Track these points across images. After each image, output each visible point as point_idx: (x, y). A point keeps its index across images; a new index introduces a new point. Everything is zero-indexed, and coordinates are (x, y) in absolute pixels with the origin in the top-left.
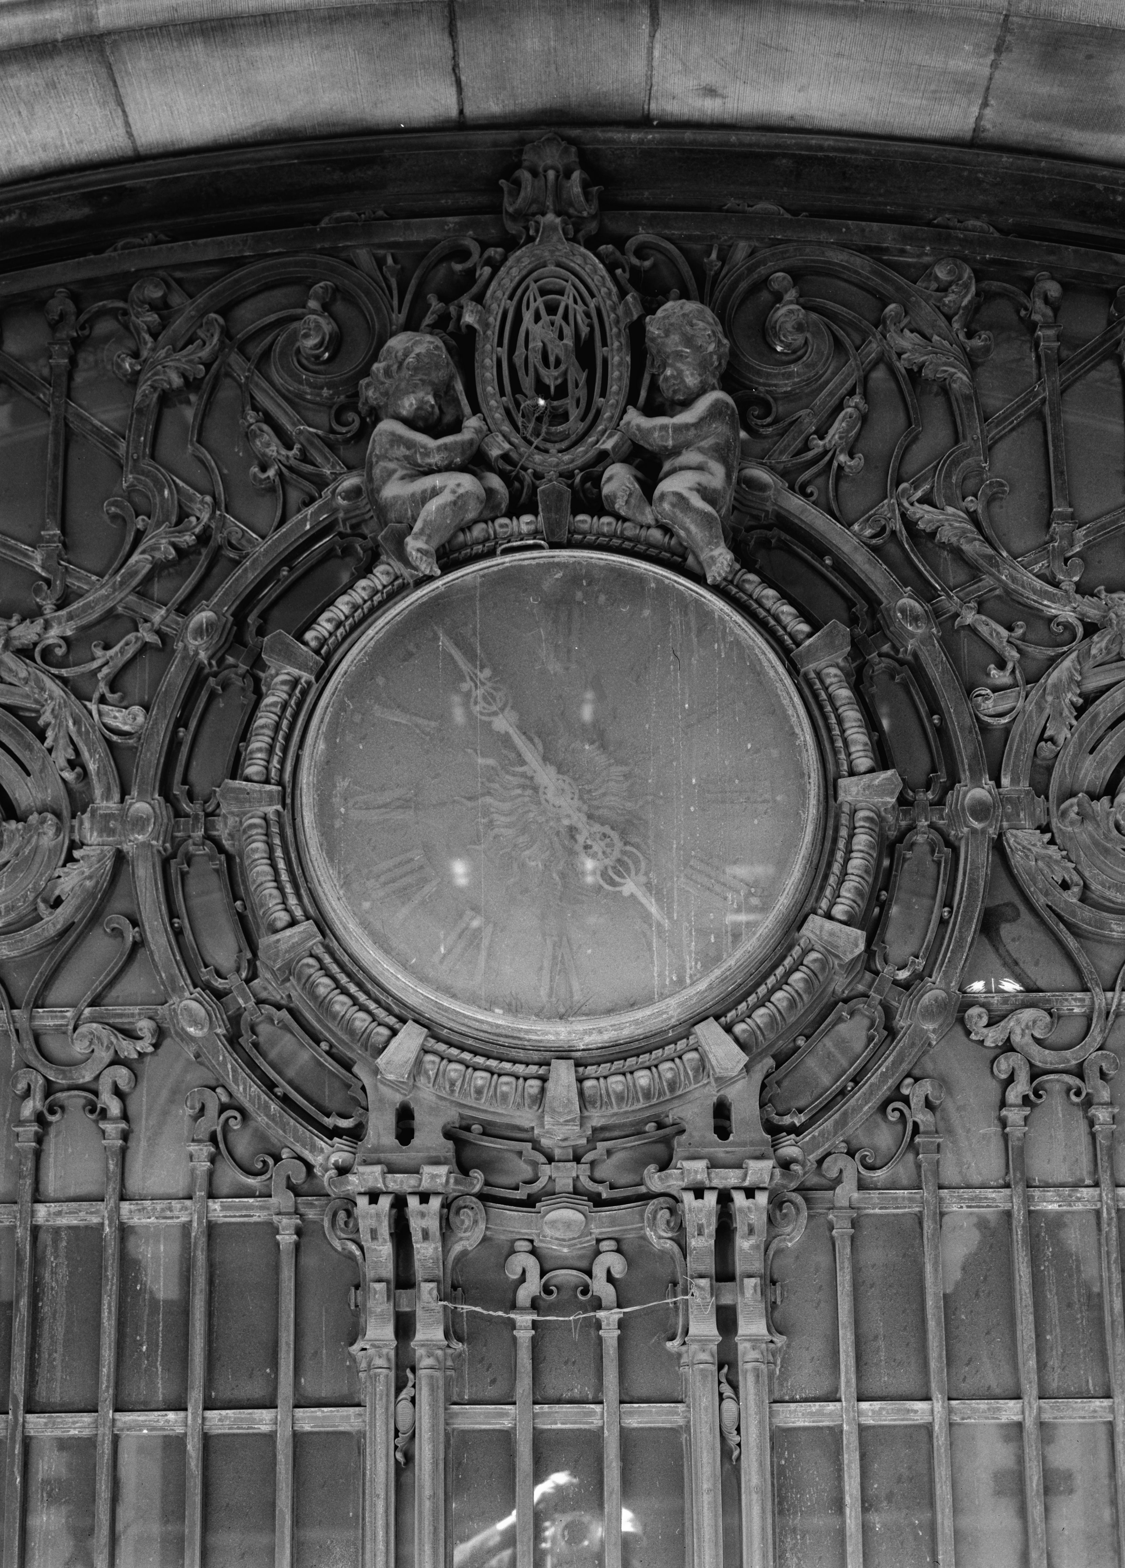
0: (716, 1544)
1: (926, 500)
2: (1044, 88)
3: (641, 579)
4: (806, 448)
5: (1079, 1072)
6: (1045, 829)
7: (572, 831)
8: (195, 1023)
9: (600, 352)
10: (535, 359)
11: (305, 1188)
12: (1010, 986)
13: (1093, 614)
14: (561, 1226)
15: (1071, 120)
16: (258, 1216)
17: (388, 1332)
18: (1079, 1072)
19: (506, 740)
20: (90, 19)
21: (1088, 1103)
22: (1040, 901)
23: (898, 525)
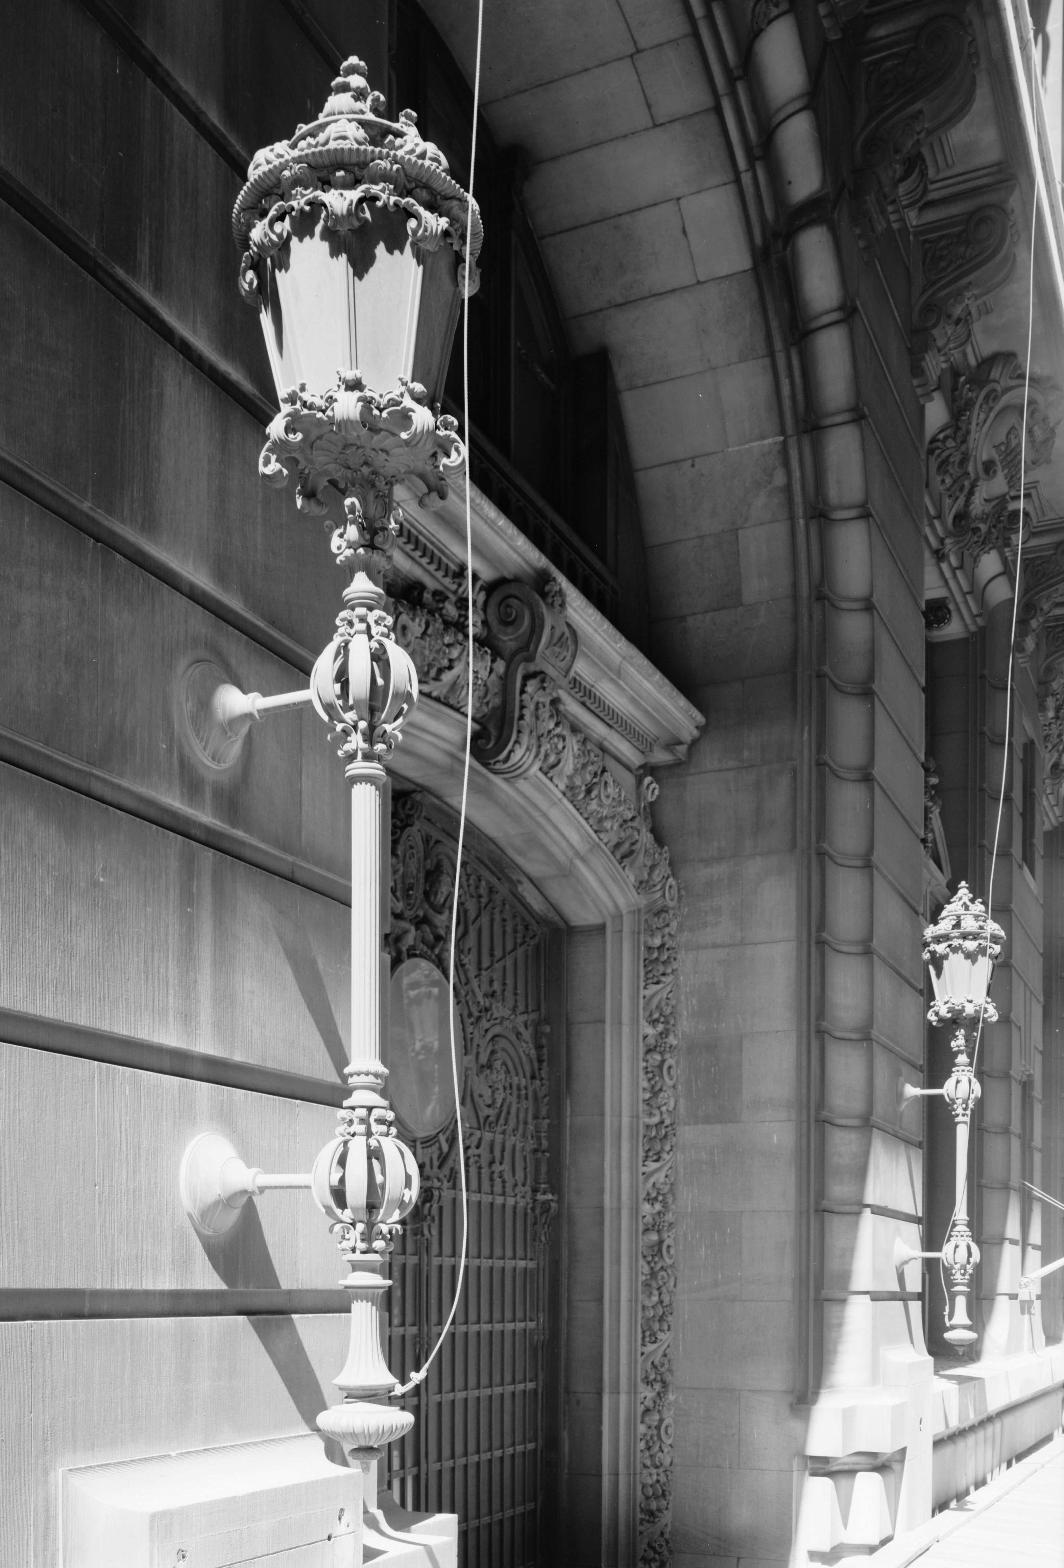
5: (479, 1156)
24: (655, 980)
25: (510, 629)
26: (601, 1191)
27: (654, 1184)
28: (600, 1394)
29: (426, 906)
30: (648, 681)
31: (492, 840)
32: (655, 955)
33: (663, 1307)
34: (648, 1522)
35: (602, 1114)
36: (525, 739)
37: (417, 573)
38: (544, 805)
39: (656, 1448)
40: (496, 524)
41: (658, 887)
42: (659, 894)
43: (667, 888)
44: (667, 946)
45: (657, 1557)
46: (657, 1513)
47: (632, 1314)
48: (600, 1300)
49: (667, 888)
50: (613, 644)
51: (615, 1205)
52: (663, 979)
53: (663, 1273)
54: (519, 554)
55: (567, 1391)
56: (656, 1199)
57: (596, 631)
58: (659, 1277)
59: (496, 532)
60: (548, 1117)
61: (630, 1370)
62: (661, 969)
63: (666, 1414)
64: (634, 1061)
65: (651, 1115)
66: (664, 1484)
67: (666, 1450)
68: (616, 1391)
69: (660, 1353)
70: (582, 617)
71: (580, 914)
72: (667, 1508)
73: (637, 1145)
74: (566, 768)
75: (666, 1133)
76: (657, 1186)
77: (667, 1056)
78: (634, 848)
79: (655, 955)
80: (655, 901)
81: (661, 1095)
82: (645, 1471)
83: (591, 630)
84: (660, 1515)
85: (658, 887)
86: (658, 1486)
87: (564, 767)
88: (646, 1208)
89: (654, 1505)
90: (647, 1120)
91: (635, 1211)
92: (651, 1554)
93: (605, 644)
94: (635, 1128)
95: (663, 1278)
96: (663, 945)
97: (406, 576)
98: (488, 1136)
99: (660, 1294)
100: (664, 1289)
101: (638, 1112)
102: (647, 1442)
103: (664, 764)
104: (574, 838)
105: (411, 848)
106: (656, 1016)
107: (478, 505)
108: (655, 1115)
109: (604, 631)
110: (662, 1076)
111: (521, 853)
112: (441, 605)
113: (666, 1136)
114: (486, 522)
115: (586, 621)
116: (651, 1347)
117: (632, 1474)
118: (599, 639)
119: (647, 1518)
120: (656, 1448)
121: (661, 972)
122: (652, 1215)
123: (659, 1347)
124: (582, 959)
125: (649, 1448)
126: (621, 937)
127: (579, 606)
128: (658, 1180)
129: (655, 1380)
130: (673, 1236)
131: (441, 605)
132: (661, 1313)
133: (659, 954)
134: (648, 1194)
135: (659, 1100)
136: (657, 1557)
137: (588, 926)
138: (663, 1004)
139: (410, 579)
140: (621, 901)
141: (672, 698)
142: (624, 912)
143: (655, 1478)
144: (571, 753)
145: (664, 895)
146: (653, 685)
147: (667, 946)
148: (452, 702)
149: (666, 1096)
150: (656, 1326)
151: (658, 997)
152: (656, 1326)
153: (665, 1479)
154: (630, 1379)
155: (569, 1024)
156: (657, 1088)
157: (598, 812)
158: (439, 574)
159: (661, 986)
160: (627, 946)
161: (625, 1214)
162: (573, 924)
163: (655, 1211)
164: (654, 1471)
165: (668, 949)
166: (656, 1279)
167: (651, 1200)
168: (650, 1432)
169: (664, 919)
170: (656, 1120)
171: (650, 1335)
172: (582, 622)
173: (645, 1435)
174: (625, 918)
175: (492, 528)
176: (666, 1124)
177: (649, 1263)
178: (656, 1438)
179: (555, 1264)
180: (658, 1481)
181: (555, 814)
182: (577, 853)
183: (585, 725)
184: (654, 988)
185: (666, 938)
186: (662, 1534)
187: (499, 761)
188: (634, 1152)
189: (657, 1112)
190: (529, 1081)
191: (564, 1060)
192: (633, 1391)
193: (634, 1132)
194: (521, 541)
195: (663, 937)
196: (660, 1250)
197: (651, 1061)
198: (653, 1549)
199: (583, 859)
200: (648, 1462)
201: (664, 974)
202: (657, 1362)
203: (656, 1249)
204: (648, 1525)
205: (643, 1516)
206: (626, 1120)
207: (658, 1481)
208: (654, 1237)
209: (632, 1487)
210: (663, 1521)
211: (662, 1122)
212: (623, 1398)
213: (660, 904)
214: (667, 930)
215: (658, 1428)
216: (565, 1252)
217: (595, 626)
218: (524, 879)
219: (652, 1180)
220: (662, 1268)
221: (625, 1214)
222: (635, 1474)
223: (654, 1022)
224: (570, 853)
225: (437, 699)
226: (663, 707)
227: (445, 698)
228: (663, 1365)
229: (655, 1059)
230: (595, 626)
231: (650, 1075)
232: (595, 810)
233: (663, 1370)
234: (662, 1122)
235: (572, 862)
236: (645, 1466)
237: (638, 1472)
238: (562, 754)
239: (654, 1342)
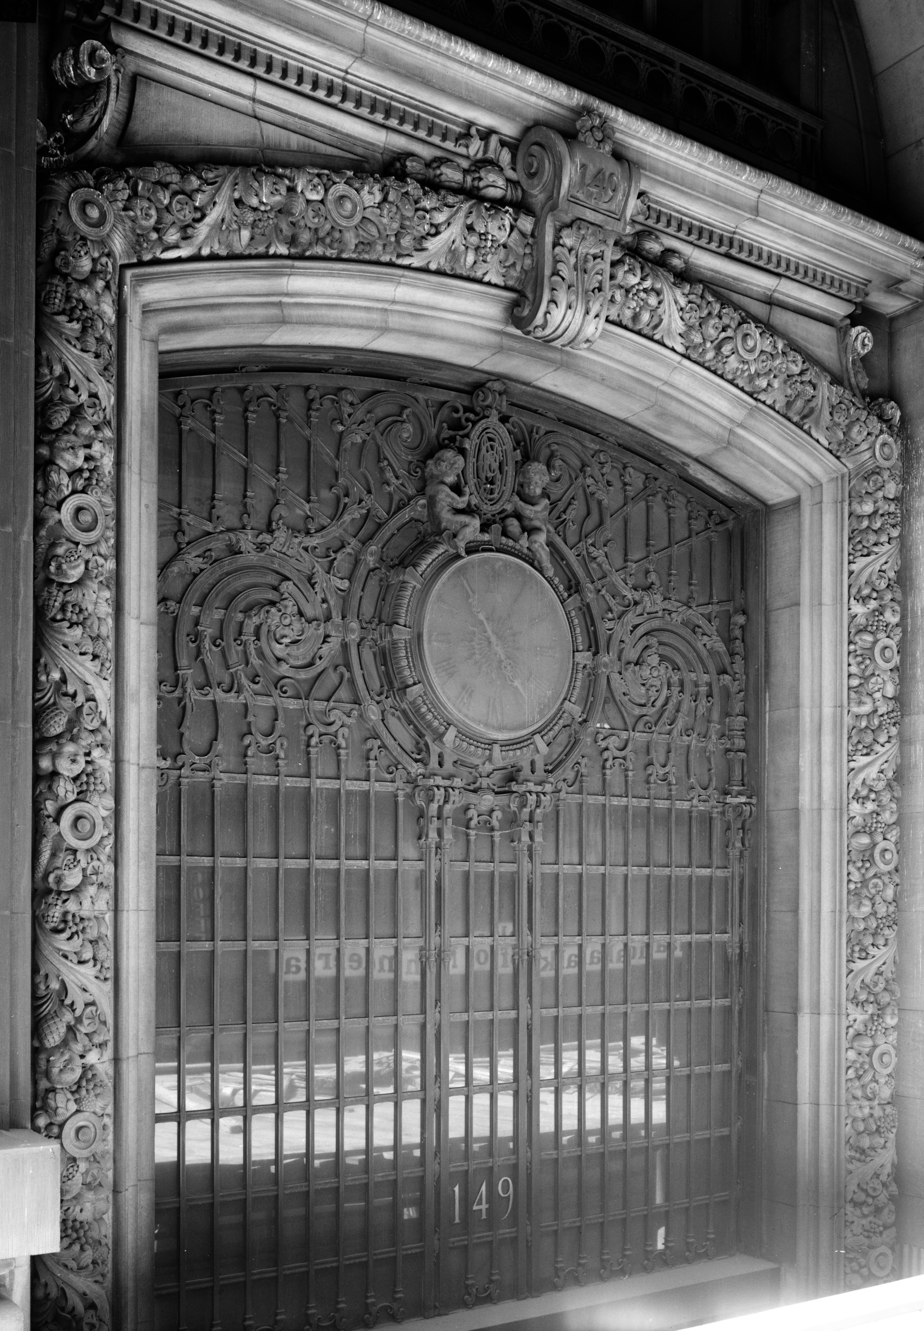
0: (767, 981)
1: (593, 545)
2: (655, 421)
3: (525, 570)
4: (559, 517)
5: (624, 758)
6: (620, 673)
7: (500, 661)
8: (374, 714)
9: (506, 468)
10: (486, 468)
11: (412, 781)
12: (607, 726)
13: (637, 598)
14: (488, 800)
15: (654, 427)
16: (391, 789)
17: (436, 835)
18: (624, 758)
19: (481, 623)
20: (386, 322)
21: (626, 770)
22: (618, 698)
23: (585, 553)
24: (865, 551)
25: (536, 181)
26: (797, 791)
27: (864, 782)
28: (795, 1013)
29: (516, 498)
30: (813, 213)
31: (624, 422)
32: (865, 523)
33: (877, 919)
34: (859, 1160)
35: (797, 706)
36: (562, 297)
37: (400, 143)
38: (662, 372)
39: (868, 1077)
40: (485, 67)
41: (864, 446)
42: (867, 455)
43: (878, 446)
44: (881, 512)
45: (870, 1200)
46: (868, 1152)
47: (836, 926)
48: (795, 910)
49: (878, 446)
50: (738, 178)
51: (815, 806)
52: (876, 549)
53: (875, 880)
54: (538, 96)
55: (767, 1010)
56: (866, 798)
57: (699, 165)
58: (871, 885)
59: (491, 76)
60: (744, 715)
61: (834, 988)
62: (873, 538)
63: (880, 1040)
64: (837, 644)
65: (860, 703)
66: (880, 1119)
67: (882, 1081)
68: (816, 1011)
69: (873, 969)
70: (671, 153)
71: (775, 492)
72: (884, 1147)
73: (841, 738)
74: (673, 326)
75: (881, 722)
76: (868, 782)
77: (881, 635)
78: (812, 404)
79: (865, 523)
80: (863, 463)
81: (873, 680)
82: (854, 1103)
83: (693, 167)
84: (873, 1153)
85: (864, 446)
86: (871, 1120)
87: (670, 324)
88: (855, 807)
89: (866, 1142)
90: (855, 709)
91: (840, 811)
92: (862, 1197)
93: (722, 179)
94: (838, 720)
95: (876, 886)
96: (875, 512)
97: (385, 148)
98: (639, 737)
99: (873, 905)
100: (878, 899)
101: (842, 701)
102: (857, 1070)
103: (903, 311)
104: (723, 405)
105: (490, 439)
106: (866, 592)
107: (448, 49)
108: (864, 703)
109: (712, 163)
110: (872, 659)
111: (665, 432)
112: (438, 172)
113: (880, 726)
114: (471, 67)
115: (680, 157)
116: (860, 964)
117: (835, 1104)
118: (710, 174)
119: (858, 1155)
120: (868, 1077)
121: (872, 542)
122: (864, 816)
123: (871, 964)
124: (780, 538)
125: (859, 1078)
126: (821, 509)
127: (657, 140)
128: (868, 775)
129: (866, 1001)
130: (893, 839)
131: (438, 172)
132: (875, 925)
133: (870, 522)
134: (857, 792)
135: (871, 686)
136: (870, 1200)
137: (785, 502)
138: (874, 578)
139: (394, 152)
140: (816, 469)
141: (863, 229)
142: (824, 480)
143: (867, 1111)
144: (674, 308)
145: (874, 455)
146: (825, 218)
147: (881, 512)
148: (459, 271)
149: (880, 680)
150: (868, 940)
151: (869, 570)
152: (868, 940)
153: (881, 1114)
154: (833, 999)
155: (767, 612)
156: (868, 673)
157: (743, 371)
158: (436, 139)
159: (872, 557)
160: (828, 519)
161: (827, 815)
162: (770, 502)
163: (867, 811)
164: (866, 1103)
165: (882, 515)
166: (867, 887)
167: (861, 799)
168: (861, 1060)
169: (875, 482)
170: (866, 709)
171: (861, 950)
172: (672, 158)
173: (854, 1062)
174: (824, 486)
175: (482, 72)
176: (880, 712)
177: (859, 869)
178: (866, 1067)
179: (755, 872)
180: (872, 1115)
181: (681, 380)
182: (731, 420)
183: (735, 279)
184: (863, 561)
185: (880, 503)
186: (877, 1175)
187: (536, 327)
188: (837, 746)
189: (868, 700)
190: (715, 677)
191: (762, 650)
192: (837, 1012)
193: (837, 723)
194: (531, 79)
195: (875, 502)
196: (872, 855)
197: (860, 643)
198: (865, 1191)
199: (741, 425)
200: (859, 1093)
201: (875, 544)
202: (867, 981)
203: (867, 854)
204: (859, 1164)
205: (853, 1153)
206: (828, 711)
207: (872, 1115)
208: (865, 840)
209: (836, 1119)
210: (878, 1161)
211: (875, 711)
212: (825, 1020)
213: (870, 465)
214: (880, 494)
215: (870, 1055)
216: (764, 859)
217: (697, 160)
218: (687, 460)
219: (862, 776)
220: (875, 876)
221: (827, 815)
222: (839, 1105)
223: (864, 600)
224: (725, 423)
225: (439, 273)
226: (852, 241)
227: (452, 269)
228: (876, 984)
229: (865, 641)
230: (697, 160)
231: (859, 659)
232: (737, 369)
233: (877, 989)
234: (875, 711)
235: (731, 431)
236: (855, 1098)
237: (843, 1102)
238: (660, 311)
239: (865, 959)
